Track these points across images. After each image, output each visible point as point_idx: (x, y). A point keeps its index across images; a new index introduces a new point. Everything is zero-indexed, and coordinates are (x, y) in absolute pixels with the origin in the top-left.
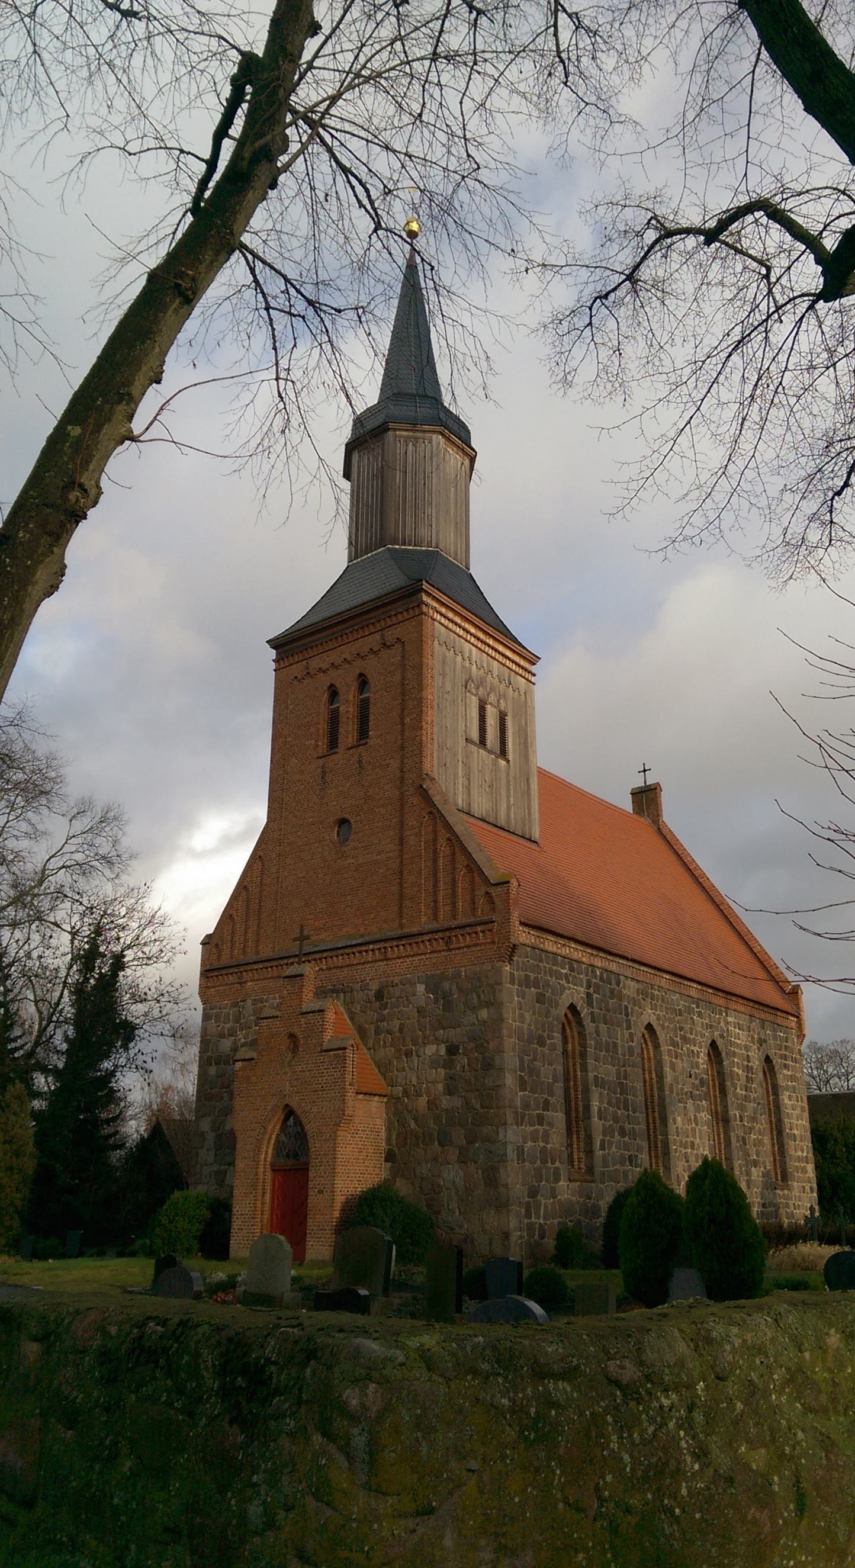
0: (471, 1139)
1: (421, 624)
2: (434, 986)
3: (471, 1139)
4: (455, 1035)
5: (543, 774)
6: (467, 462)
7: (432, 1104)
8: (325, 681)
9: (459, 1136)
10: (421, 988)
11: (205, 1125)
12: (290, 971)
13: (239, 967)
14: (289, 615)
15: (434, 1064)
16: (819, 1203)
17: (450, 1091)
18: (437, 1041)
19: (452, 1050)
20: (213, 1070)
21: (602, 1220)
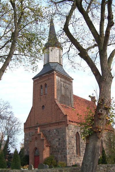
0: (62, 151)
1: (54, 76)
2: (57, 130)
3: (62, 151)
4: (59, 137)
5: (74, 95)
6: (70, 28)
7: (57, 147)
8: (40, 84)
9: (60, 151)
10: (55, 130)
11: (25, 150)
12: (36, 128)
13: (29, 128)
14: (33, 77)
15: (57, 141)
16: (28, 126)
17: (59, 145)
18: (57, 138)
19: (59, 139)
20: (26, 142)
21: (82, 162)
